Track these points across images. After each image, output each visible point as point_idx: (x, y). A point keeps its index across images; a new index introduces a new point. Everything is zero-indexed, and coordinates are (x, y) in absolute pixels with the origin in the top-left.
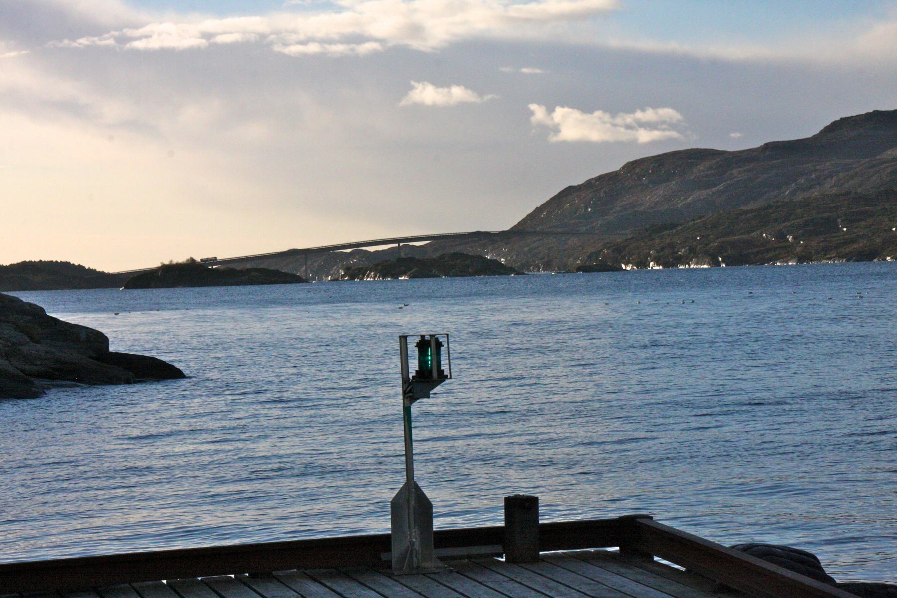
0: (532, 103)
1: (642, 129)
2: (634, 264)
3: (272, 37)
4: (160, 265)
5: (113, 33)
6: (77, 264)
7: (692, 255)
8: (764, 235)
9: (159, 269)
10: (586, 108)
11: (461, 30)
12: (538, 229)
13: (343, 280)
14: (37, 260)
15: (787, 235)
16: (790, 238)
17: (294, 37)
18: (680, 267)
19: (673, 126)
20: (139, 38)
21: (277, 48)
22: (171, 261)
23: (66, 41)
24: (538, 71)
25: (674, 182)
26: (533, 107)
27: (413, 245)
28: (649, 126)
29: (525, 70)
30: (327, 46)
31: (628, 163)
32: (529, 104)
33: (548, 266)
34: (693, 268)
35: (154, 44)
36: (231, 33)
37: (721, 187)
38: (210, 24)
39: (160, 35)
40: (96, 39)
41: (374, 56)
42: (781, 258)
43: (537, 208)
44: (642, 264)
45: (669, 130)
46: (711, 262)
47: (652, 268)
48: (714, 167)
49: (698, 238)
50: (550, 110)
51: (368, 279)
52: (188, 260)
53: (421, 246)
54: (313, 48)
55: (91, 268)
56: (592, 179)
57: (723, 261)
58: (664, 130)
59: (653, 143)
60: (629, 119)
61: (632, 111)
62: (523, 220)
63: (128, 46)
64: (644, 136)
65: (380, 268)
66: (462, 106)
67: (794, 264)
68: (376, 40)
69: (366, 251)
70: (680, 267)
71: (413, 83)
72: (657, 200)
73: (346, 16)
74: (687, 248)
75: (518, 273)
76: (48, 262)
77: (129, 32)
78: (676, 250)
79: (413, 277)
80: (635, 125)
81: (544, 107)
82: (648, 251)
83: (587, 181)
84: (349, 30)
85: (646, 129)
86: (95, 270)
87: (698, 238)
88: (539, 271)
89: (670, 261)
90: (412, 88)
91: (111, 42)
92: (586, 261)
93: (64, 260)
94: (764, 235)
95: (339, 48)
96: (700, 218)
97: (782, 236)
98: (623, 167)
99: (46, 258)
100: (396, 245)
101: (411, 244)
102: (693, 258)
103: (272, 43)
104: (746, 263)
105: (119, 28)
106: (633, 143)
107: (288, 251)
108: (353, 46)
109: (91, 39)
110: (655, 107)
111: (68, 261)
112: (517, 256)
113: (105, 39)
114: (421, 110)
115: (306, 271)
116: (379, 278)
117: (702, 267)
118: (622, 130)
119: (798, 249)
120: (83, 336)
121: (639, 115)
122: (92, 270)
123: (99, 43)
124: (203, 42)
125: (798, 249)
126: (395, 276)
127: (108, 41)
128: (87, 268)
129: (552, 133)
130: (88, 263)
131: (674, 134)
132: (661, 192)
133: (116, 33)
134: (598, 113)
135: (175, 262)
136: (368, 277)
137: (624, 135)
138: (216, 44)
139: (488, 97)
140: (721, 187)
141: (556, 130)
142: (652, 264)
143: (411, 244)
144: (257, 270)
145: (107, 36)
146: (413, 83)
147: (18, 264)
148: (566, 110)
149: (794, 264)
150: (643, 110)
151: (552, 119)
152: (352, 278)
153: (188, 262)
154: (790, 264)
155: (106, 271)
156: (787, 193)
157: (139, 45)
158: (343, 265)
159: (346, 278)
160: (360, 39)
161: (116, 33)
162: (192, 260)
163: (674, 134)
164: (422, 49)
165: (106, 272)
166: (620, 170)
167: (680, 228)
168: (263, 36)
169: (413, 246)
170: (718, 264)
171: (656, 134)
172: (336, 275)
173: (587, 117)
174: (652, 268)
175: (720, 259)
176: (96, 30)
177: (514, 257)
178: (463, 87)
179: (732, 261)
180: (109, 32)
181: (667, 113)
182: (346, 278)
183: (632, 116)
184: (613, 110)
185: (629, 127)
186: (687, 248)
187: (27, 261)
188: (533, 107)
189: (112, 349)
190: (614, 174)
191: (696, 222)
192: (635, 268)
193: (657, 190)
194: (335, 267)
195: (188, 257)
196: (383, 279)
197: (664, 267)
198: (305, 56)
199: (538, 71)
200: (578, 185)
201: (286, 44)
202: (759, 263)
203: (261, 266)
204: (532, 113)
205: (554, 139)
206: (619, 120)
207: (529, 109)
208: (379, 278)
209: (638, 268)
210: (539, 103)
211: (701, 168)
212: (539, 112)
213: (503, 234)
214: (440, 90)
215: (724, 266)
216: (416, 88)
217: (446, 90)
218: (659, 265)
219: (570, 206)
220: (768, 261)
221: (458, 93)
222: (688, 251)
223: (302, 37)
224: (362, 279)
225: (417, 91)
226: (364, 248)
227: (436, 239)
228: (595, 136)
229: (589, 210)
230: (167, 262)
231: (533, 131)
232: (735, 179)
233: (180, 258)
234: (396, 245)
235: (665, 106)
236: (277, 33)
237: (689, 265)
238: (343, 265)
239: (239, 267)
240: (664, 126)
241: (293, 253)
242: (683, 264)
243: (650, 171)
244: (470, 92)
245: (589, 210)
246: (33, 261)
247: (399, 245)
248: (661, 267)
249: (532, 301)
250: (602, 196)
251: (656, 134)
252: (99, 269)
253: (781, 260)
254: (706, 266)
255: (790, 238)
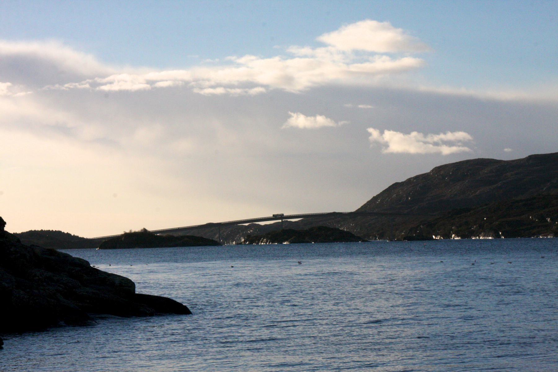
0: (370, 127)
1: (444, 145)
2: (441, 236)
3: (193, 83)
4: (123, 233)
5: (88, 80)
6: (66, 232)
7: (481, 230)
8: (531, 217)
9: (122, 235)
10: (405, 130)
11: (318, 79)
12: (375, 211)
13: (245, 244)
14: (39, 230)
15: (547, 217)
16: (549, 220)
17: (207, 83)
18: (473, 238)
19: (464, 143)
20: (105, 84)
21: (196, 91)
22: (131, 231)
23: (57, 86)
24: (369, 107)
25: (467, 181)
26: (371, 130)
27: (290, 221)
28: (450, 143)
29: (360, 106)
30: (229, 90)
31: (436, 167)
32: (367, 128)
33: (382, 236)
34: (482, 239)
35: (115, 87)
36: (167, 81)
37: (499, 184)
38: (153, 75)
39: (119, 82)
40: (77, 84)
41: (261, 96)
42: (543, 233)
43: (374, 197)
44: (447, 236)
45: (463, 146)
46: (494, 235)
47: (454, 238)
48: (494, 171)
49: (485, 219)
50: (382, 133)
51: (262, 244)
52: (142, 230)
53: (295, 222)
54: (220, 91)
55: (75, 235)
56: (411, 178)
57: (503, 235)
58: (459, 146)
59: (452, 155)
60: (436, 138)
61: (438, 133)
62: (365, 205)
63: (97, 89)
64: (446, 150)
65: (270, 236)
66: (324, 129)
67: (552, 237)
68: (262, 86)
69: (258, 224)
70: (473, 238)
71: (290, 113)
72: (456, 192)
73: (242, 70)
74: (478, 225)
75: (363, 241)
76: (47, 231)
77: (98, 80)
78: (470, 226)
79: (292, 242)
80: (440, 143)
81: (422, 134)
82: (450, 227)
83: (407, 179)
84: (245, 79)
85: (446, 145)
86: (78, 236)
87: (485, 219)
88: (376, 239)
89: (466, 234)
90: (290, 116)
91: (87, 86)
92: (408, 233)
93: (57, 230)
94: (531, 217)
95: (238, 91)
96: (486, 205)
97: (543, 219)
98: (433, 170)
99: (46, 228)
100: (280, 221)
101: (289, 220)
102: (482, 232)
103: (193, 87)
104: (519, 236)
105: (92, 78)
106: (439, 154)
107: (207, 224)
108: (247, 89)
109: (74, 84)
110: (453, 131)
111: (60, 230)
112: (361, 229)
113: (82, 84)
114: (296, 132)
115: (219, 237)
116: (269, 243)
117: (488, 238)
118: (431, 146)
119: (554, 227)
120: (117, 282)
121: (442, 136)
122: (76, 236)
123: (79, 87)
124: (148, 86)
125: (554, 227)
126: (280, 242)
127: (85, 86)
128: (72, 235)
129: (384, 148)
130: (74, 232)
131: (466, 149)
132: (458, 187)
133: (90, 81)
134: (414, 134)
135: (133, 231)
136: (262, 242)
137: (431, 149)
138: (156, 88)
139: (341, 123)
140: (499, 184)
141: (386, 145)
142: (453, 236)
143: (289, 220)
144: (188, 237)
145: (83, 82)
146: (290, 113)
147: (27, 232)
148: (392, 132)
149: (552, 237)
150: (445, 133)
151: (383, 138)
152: (251, 243)
153: (142, 231)
154: (549, 237)
155: (85, 237)
156: (544, 189)
157: (106, 88)
158: (243, 234)
159: (247, 243)
160: (252, 85)
161: (90, 81)
162: (145, 230)
163: (466, 149)
164: (293, 91)
165: (85, 238)
166: (430, 172)
167: (472, 212)
168: (187, 83)
169: (290, 221)
170: (499, 237)
171: (454, 149)
172: (238, 240)
173: (406, 137)
174: (454, 238)
175: (500, 233)
176: (79, 78)
177: (359, 230)
178: (324, 117)
179: (508, 235)
180: (85, 80)
181: (461, 135)
182: (247, 243)
183: (438, 136)
184: (426, 130)
185: (436, 144)
186: (478, 225)
187: (33, 230)
188: (371, 130)
189: (138, 291)
190: (426, 175)
191: (483, 208)
192: (442, 238)
193: (455, 186)
194: (238, 235)
195: (142, 228)
196: (272, 243)
197: (462, 238)
198: (214, 96)
199: (369, 107)
200: (402, 182)
201: (202, 88)
202: (527, 237)
203: (188, 235)
204: (370, 134)
205: (385, 151)
206: (429, 139)
207: (367, 132)
208: (269, 243)
209: (444, 238)
210: (374, 128)
211: (485, 172)
212: (374, 133)
213: (351, 214)
214: (309, 118)
215: (503, 238)
216: (293, 117)
217: (313, 118)
218: (458, 236)
219: (396, 196)
220: (533, 235)
221: (321, 120)
222: (478, 227)
223: (213, 83)
224: (258, 244)
225: (293, 119)
226: (257, 223)
227: (306, 217)
228: (413, 149)
229: (410, 198)
230: (128, 231)
231: (371, 146)
232: (509, 179)
233: (137, 228)
234: (280, 221)
235: (460, 130)
236: (196, 80)
237: (479, 237)
238: (243, 234)
239: (176, 235)
240: (459, 144)
241: (210, 226)
242: (475, 236)
243: (451, 173)
244: (329, 120)
245: (410, 198)
246: (37, 230)
247: (282, 221)
248: (460, 238)
249: (348, 259)
250: (418, 189)
251: (454, 149)
252: (81, 236)
253: (543, 235)
254: (490, 238)
255: (549, 220)
